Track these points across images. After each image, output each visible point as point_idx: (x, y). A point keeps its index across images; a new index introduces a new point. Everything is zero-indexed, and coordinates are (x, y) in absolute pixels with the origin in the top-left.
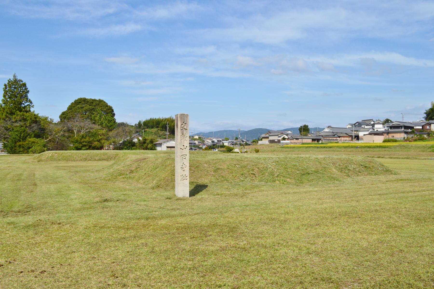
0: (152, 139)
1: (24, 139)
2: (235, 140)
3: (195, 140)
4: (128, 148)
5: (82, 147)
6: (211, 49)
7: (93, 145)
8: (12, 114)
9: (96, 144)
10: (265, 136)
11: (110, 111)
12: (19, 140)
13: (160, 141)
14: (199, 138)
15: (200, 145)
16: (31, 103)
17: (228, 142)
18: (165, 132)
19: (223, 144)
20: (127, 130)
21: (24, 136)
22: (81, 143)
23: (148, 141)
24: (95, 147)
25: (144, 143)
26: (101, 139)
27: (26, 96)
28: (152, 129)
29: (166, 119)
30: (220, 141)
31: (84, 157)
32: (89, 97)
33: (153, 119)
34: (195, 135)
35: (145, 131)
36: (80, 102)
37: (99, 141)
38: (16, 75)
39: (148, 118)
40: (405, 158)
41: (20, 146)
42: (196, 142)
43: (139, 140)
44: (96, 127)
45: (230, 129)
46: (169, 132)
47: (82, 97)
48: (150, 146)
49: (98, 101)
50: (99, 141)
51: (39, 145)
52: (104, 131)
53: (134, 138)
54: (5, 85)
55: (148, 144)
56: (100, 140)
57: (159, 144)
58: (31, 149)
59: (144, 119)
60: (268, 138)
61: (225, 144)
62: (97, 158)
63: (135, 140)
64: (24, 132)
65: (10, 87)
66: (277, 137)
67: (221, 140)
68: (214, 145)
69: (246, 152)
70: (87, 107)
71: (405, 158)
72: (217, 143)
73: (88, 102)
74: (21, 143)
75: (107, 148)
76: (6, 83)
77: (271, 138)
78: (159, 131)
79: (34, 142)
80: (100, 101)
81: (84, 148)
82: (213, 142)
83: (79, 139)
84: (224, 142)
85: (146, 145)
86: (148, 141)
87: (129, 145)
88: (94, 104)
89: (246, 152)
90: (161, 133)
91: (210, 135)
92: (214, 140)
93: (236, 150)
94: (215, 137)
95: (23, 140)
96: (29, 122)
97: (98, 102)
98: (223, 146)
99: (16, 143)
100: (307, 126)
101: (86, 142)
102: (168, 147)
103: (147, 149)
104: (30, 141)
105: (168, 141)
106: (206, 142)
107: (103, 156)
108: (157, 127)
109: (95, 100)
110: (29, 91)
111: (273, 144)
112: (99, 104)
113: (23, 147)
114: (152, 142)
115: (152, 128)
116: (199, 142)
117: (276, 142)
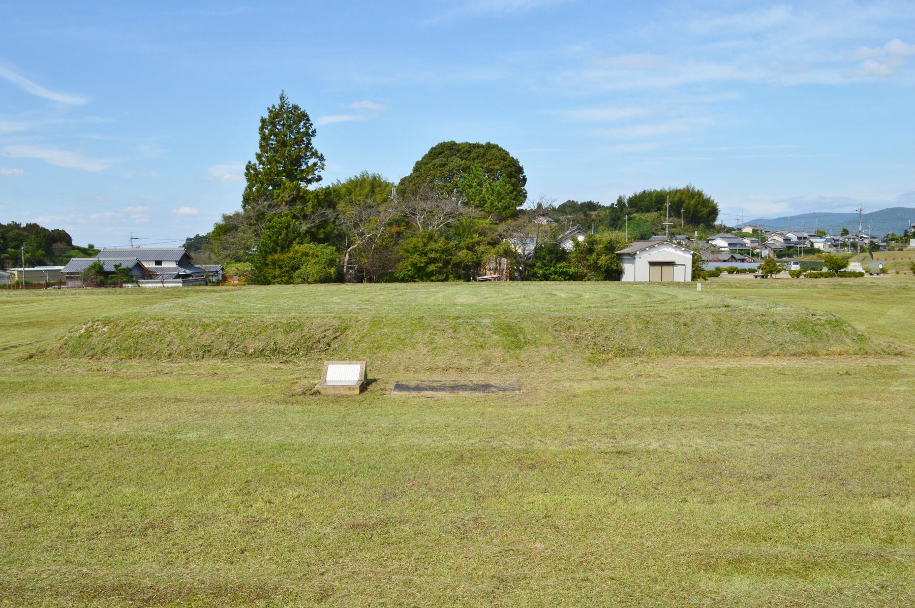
0: (610, 242)
1: (286, 246)
2: (842, 235)
3: (746, 235)
7: (455, 259)
11: (514, 173)
12: (273, 248)
13: (636, 245)
14: (754, 231)
15: (755, 248)
16: (321, 158)
17: (823, 240)
19: (812, 244)
20: (593, 217)
22: (425, 254)
23: (599, 247)
24: (461, 263)
25: (590, 251)
26: (479, 243)
28: (647, 215)
30: (805, 238)
31: (205, 339)
32: (460, 139)
33: (650, 194)
34: (745, 225)
35: (630, 219)
36: (441, 153)
38: (287, 94)
39: (639, 191)
41: (274, 263)
42: (747, 241)
43: (577, 244)
44: (470, 211)
46: (685, 218)
47: (447, 139)
49: (482, 146)
50: (470, 248)
51: (317, 259)
52: (485, 223)
53: (564, 239)
54: (263, 121)
55: (599, 255)
56: (473, 246)
57: (629, 254)
58: (298, 272)
61: (816, 246)
62: (253, 346)
63: (568, 245)
64: (287, 228)
67: (806, 235)
68: (789, 248)
69: (883, 271)
70: (456, 161)
72: (796, 243)
73: (459, 151)
74: (276, 256)
75: (493, 266)
76: (266, 115)
79: (307, 254)
80: (489, 147)
82: (787, 240)
83: (420, 245)
84: (813, 240)
85: (594, 256)
86: (599, 247)
87: (548, 257)
88: (473, 155)
89: (883, 271)
91: (782, 223)
92: (790, 235)
93: (854, 266)
95: (283, 248)
97: (482, 151)
98: (812, 251)
101: (436, 251)
102: (652, 264)
104: (297, 252)
105: (653, 247)
106: (770, 241)
107: (280, 337)
108: (659, 209)
109: (477, 146)
110: (314, 131)
114: (610, 248)
115: (648, 211)
116: (752, 242)
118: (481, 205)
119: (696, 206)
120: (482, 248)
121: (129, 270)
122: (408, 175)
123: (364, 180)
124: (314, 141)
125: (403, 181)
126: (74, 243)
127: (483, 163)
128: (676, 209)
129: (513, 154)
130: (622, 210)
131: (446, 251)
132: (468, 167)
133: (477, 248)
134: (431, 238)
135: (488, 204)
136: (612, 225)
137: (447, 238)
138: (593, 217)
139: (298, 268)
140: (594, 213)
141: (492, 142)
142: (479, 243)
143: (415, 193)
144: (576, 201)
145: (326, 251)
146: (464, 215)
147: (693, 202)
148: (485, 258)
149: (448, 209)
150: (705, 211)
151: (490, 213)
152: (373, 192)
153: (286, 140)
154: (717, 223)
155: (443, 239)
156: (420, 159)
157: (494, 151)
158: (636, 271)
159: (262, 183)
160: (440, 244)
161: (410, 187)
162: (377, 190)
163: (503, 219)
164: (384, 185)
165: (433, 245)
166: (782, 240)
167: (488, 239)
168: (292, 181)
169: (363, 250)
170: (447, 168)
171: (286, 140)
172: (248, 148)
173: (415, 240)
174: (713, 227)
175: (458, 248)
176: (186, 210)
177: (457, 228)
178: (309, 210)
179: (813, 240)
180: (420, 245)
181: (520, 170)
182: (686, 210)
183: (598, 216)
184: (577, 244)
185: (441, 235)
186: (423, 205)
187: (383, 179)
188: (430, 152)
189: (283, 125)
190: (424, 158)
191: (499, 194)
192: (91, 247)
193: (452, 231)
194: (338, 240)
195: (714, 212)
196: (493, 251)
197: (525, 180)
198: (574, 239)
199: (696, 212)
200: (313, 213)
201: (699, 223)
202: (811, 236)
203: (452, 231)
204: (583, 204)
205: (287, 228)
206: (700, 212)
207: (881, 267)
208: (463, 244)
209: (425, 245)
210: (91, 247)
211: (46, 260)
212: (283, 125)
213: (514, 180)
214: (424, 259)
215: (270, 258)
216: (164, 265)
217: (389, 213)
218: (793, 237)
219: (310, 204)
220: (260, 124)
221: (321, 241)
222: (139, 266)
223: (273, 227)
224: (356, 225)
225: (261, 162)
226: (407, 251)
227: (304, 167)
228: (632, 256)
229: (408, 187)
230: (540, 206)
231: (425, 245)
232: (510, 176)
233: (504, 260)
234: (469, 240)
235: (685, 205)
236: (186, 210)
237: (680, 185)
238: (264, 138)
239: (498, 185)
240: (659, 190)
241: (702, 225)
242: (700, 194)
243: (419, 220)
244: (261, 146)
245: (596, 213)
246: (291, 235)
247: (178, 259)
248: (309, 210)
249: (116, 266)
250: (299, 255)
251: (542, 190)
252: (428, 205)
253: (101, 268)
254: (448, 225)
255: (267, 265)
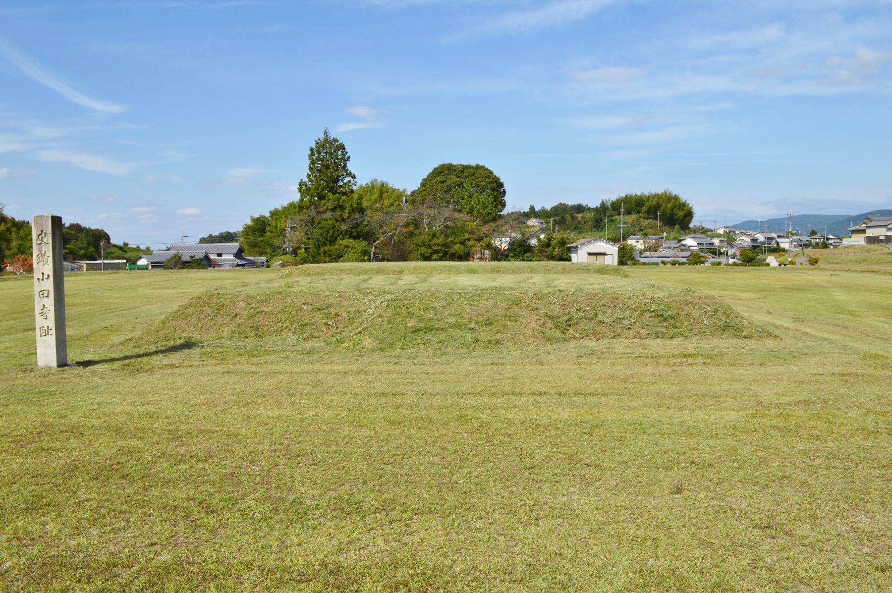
1: (333, 241)
3: (719, 236)
4: (517, 257)
5: (432, 254)
6: (773, 32)
7: (452, 251)
8: (321, 197)
9: (457, 247)
10: (858, 228)
11: (497, 188)
15: (722, 247)
16: (354, 177)
18: (654, 221)
19: (778, 244)
20: (579, 219)
21: (332, 236)
22: (430, 247)
25: (548, 245)
26: (468, 239)
27: (345, 166)
29: (656, 195)
30: (772, 239)
32: (455, 162)
36: (441, 172)
37: (462, 243)
38: (329, 131)
40: (157, 352)
41: (325, 253)
43: (539, 240)
44: (462, 216)
45: (817, 213)
47: (446, 162)
48: (557, 252)
49: (473, 167)
50: (462, 243)
54: (312, 150)
55: (554, 248)
59: (612, 196)
60: (863, 231)
61: (782, 245)
64: (333, 228)
65: (319, 153)
66: (885, 229)
67: (774, 235)
71: (157, 352)
72: (763, 243)
73: (455, 171)
74: (326, 248)
75: (479, 256)
76: (314, 146)
77: (871, 233)
78: (641, 220)
79: (348, 247)
80: (478, 167)
81: (435, 256)
82: (754, 240)
84: (779, 240)
85: (550, 249)
86: (553, 243)
88: (466, 174)
90: (645, 223)
91: (748, 226)
94: (762, 232)
95: (331, 242)
96: (347, 211)
97: (472, 171)
99: (319, 246)
100: (60, 218)
101: (438, 245)
102: (590, 254)
103: (552, 258)
104: (341, 245)
105: (589, 242)
106: (738, 241)
108: (639, 212)
111: (873, 246)
112: (474, 174)
113: (330, 256)
114: (562, 243)
116: (721, 241)
117: (881, 241)
118: (471, 212)
119: (672, 210)
120: (471, 243)
121: (201, 260)
122: (416, 188)
123: (373, 187)
124: (349, 164)
125: (413, 193)
126: (112, 242)
127: (473, 180)
128: (652, 212)
129: (497, 173)
130: (605, 213)
131: (445, 245)
132: (462, 184)
133: (467, 243)
134: (434, 235)
135: (475, 212)
136: (595, 227)
137: (446, 236)
138: (579, 219)
139: (342, 256)
140: (580, 216)
141: (480, 164)
142: (468, 239)
143: (423, 202)
144: (567, 203)
145: (360, 244)
146: (461, 212)
147: (669, 206)
148: (472, 250)
149: (447, 215)
150: (681, 214)
151: (477, 217)
152: (381, 197)
153: (329, 161)
154: (691, 225)
155: (443, 236)
156: (425, 177)
157: (481, 171)
158: (579, 257)
159: (313, 196)
160: (441, 240)
161: (419, 198)
162: (384, 195)
163: (485, 222)
164: (390, 191)
165: (435, 241)
166: (749, 240)
167: (475, 237)
168: (334, 194)
169: (386, 244)
170: (446, 184)
171: (329, 161)
172: (301, 170)
173: (423, 237)
174: (689, 228)
175: (453, 243)
176: (192, 211)
177: (453, 228)
178: (346, 216)
179: (779, 240)
180: (427, 240)
181: (501, 185)
182: (663, 213)
183: (583, 218)
184: (539, 240)
185: (442, 233)
186: (429, 211)
187: (390, 185)
188: (433, 172)
189: (326, 153)
190: (428, 176)
191: (484, 204)
192: (126, 244)
193: (449, 231)
194: (367, 236)
195: (689, 215)
196: (479, 245)
197: (504, 192)
198: (538, 237)
199: (672, 215)
200: (349, 217)
201: (675, 225)
202: (779, 237)
203: (449, 231)
204: (573, 207)
205: (333, 228)
206: (676, 215)
207: (790, 259)
208: (457, 240)
209: (430, 241)
210: (126, 244)
211: (96, 255)
212: (326, 153)
213: (496, 193)
214: (429, 251)
215: (322, 249)
216: (224, 257)
217: (403, 217)
218: (761, 237)
219: (347, 211)
220: (309, 152)
221: (355, 238)
222: (207, 257)
223: (323, 228)
224: (381, 227)
225: (310, 181)
226: (417, 245)
227: (341, 183)
228: (576, 248)
229: (415, 199)
230: (532, 208)
231: (430, 241)
232: (493, 190)
233: (487, 252)
234: (462, 238)
235: (662, 208)
236: (192, 211)
237: (659, 190)
238: (313, 162)
239: (483, 198)
240: (639, 194)
241: (677, 227)
242: (676, 198)
243: (426, 221)
244: (310, 169)
245: (581, 215)
246: (336, 233)
247: (235, 252)
248: (346, 216)
249: (191, 257)
250: (342, 247)
251: (515, 202)
252: (432, 212)
253: (180, 258)
254: (446, 227)
255: (319, 254)
